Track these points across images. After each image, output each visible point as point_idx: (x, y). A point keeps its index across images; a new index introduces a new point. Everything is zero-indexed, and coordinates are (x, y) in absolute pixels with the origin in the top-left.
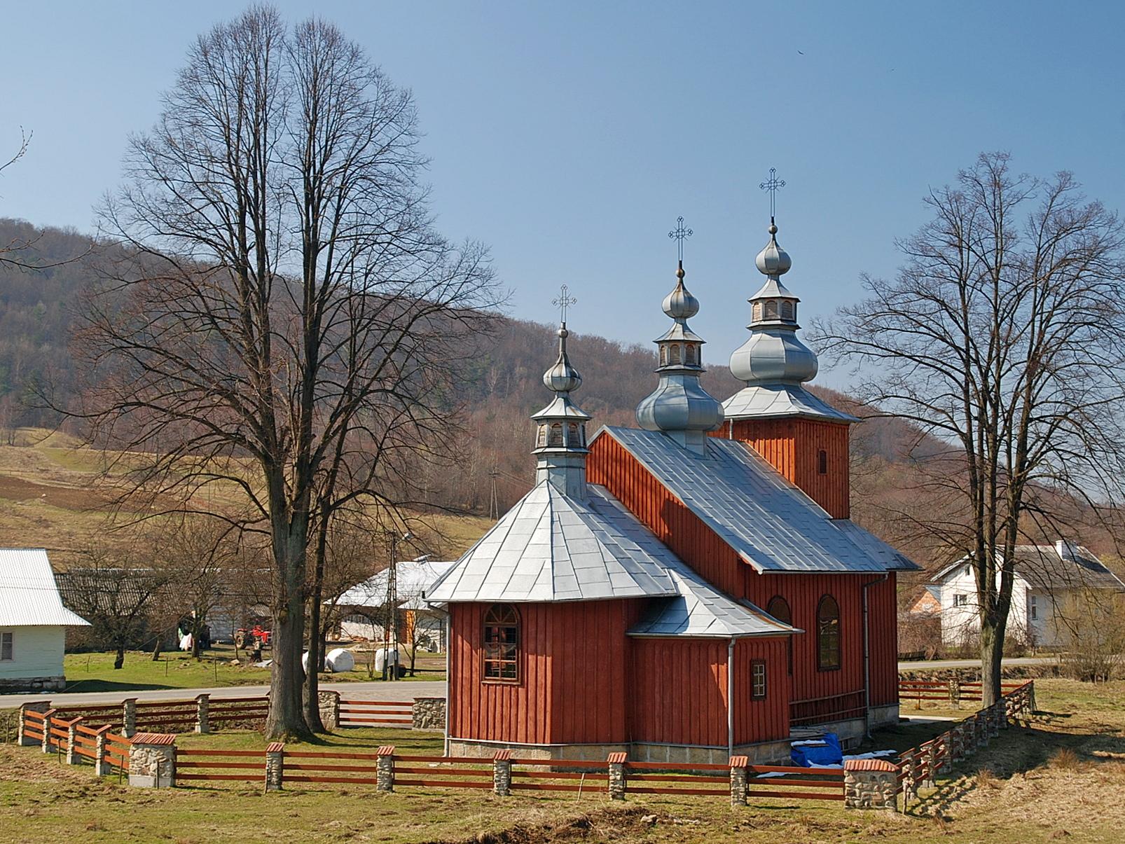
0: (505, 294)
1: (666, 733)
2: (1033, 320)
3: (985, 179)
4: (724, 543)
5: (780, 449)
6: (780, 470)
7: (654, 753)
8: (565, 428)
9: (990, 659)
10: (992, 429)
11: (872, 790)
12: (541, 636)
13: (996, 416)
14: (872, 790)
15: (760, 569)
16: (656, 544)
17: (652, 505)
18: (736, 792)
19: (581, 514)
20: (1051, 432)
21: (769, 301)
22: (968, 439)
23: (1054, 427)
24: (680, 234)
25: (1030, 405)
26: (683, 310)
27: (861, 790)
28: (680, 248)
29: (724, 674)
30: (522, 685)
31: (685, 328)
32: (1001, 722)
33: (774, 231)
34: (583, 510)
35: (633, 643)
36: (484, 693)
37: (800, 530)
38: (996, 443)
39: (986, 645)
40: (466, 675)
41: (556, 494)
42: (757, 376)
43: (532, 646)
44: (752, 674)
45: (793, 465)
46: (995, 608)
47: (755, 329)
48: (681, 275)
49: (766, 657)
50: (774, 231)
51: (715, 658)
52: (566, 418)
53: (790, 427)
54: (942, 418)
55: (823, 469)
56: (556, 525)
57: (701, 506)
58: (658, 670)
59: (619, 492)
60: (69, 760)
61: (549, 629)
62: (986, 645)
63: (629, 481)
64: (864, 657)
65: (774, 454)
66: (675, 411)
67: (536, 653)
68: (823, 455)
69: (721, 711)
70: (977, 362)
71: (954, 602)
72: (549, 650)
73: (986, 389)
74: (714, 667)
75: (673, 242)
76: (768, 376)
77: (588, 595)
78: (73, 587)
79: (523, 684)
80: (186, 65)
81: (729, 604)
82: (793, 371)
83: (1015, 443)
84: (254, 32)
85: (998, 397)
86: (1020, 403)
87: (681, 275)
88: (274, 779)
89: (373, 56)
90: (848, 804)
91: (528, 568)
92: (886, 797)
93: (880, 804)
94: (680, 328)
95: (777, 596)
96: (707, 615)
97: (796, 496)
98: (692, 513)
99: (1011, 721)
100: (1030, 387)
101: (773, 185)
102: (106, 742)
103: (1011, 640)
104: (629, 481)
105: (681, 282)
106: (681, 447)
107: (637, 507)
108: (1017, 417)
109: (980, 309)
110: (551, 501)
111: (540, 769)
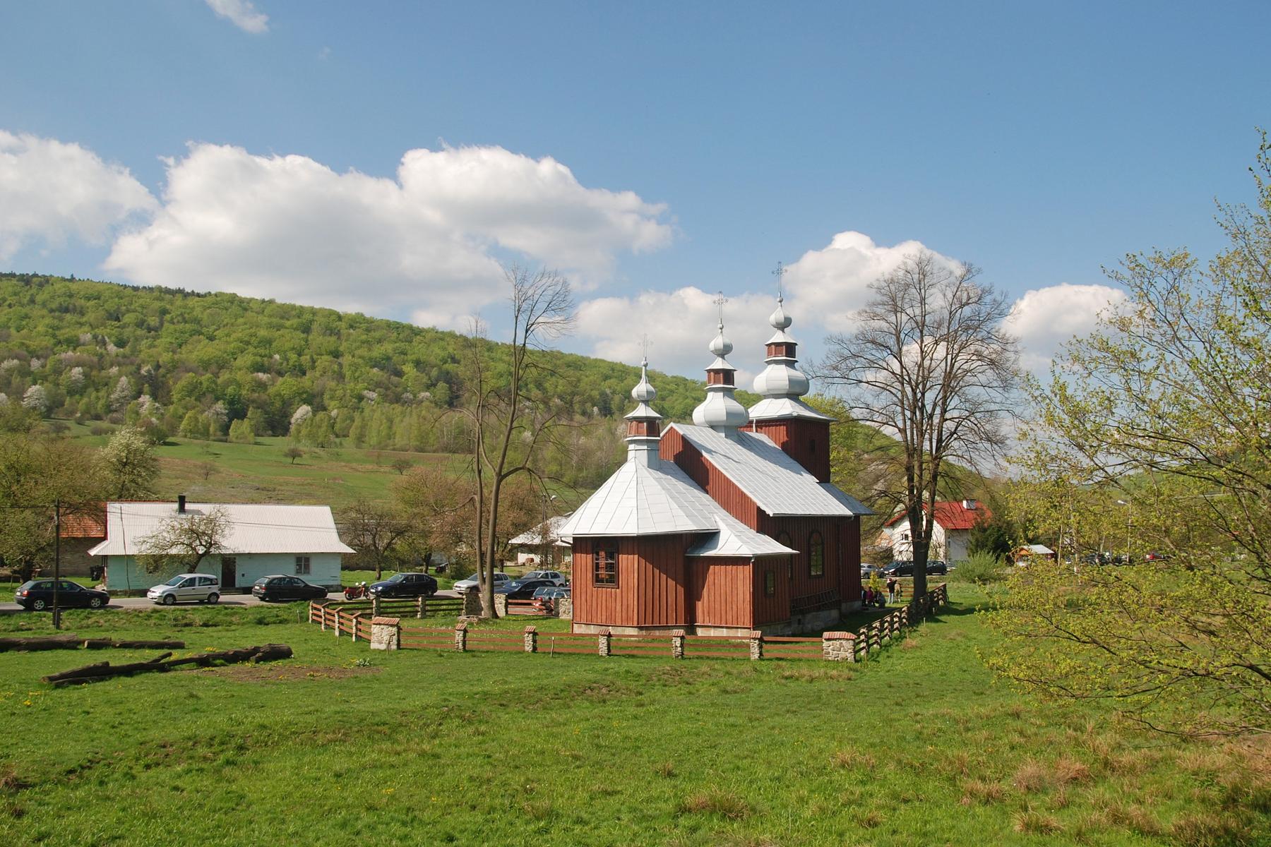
22: (903, 431)
23: (959, 425)
25: (944, 411)
38: (922, 434)
46: (921, 541)
60: (337, 633)
70: (910, 383)
71: (898, 539)
73: (915, 400)
78: (347, 530)
85: (923, 405)
86: (938, 411)
100: (945, 398)
102: (359, 623)
108: (936, 420)
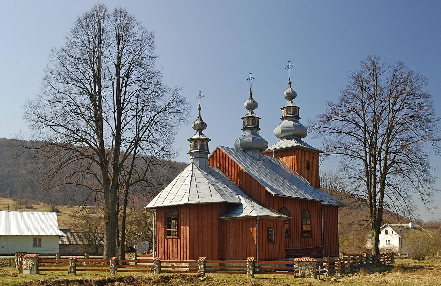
0: (189, 106)
1: (234, 256)
2: (389, 114)
3: (370, 65)
4: (261, 185)
5: (291, 160)
6: (291, 168)
7: (228, 264)
8: (199, 143)
9: (374, 240)
10: (374, 157)
11: (305, 270)
12: (185, 219)
13: (375, 152)
14: (305, 270)
15: (273, 194)
16: (235, 187)
17: (235, 173)
18: (249, 272)
19: (204, 174)
20: (395, 157)
21: (288, 108)
22: (365, 161)
24: (251, 79)
26: (252, 106)
27: (301, 270)
28: (251, 84)
29: (255, 231)
30: (179, 238)
31: (252, 113)
32: (378, 262)
33: (290, 83)
34: (205, 173)
35: (222, 221)
36: (166, 242)
37: (295, 185)
39: (373, 236)
40: (160, 236)
41: (195, 167)
42: (284, 135)
43: (182, 223)
44: (268, 232)
45: (296, 165)
47: (283, 119)
48: (251, 94)
49: (275, 226)
50: (290, 83)
51: (252, 225)
52: (199, 139)
53: (295, 151)
54: (357, 155)
55: (308, 168)
56: (193, 178)
57: (253, 173)
58: (231, 232)
59: (224, 169)
61: (188, 215)
62: (373, 236)
63: (227, 165)
64: (322, 234)
65: (289, 162)
66: (249, 143)
67: (184, 226)
68: (308, 164)
69: (254, 246)
72: (188, 224)
74: (251, 229)
75: (248, 82)
76: (286, 134)
77: (202, 201)
79: (179, 238)
80: (74, 26)
81: (261, 207)
82: (296, 132)
83: (382, 163)
84: (98, 14)
87: (251, 94)
88: (72, 270)
89: (138, 18)
90: (295, 276)
91: (181, 193)
92: (311, 273)
93: (309, 275)
94: (250, 112)
95: (284, 207)
96: (249, 209)
97: (296, 176)
98: (249, 175)
99: (383, 263)
101: (290, 67)
103: (287, 114)
104: (227, 165)
105: (251, 96)
106: (250, 156)
107: (230, 175)
109: (369, 114)
110: (192, 170)
111: (185, 269)
